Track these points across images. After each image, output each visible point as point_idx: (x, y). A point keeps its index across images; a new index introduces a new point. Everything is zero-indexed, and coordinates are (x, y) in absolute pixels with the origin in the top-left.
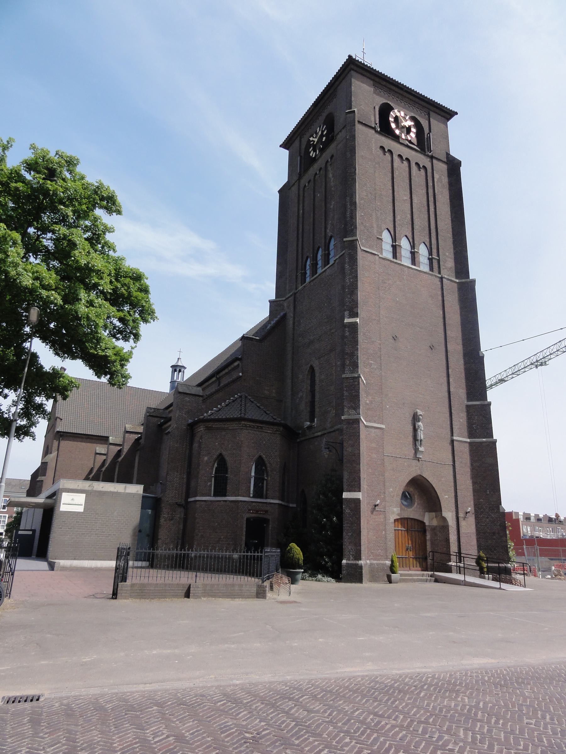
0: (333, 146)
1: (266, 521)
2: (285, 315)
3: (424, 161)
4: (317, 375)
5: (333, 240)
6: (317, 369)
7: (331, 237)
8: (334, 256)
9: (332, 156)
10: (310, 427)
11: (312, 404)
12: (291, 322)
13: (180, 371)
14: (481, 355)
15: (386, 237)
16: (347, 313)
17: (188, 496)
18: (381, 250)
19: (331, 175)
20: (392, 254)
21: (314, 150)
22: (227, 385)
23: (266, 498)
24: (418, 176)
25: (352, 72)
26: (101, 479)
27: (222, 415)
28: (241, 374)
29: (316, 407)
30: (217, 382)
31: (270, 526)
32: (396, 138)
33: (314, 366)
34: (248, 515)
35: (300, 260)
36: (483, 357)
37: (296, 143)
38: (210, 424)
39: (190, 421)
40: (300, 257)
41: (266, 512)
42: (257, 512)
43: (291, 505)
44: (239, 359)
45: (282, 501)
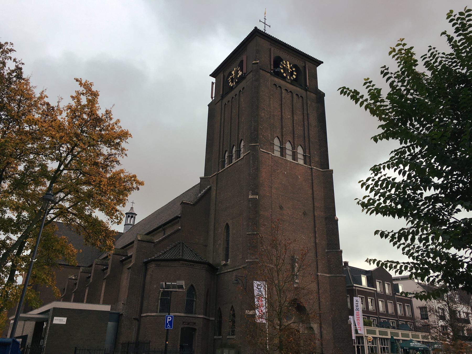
0: (244, 81)
1: (195, 330)
2: (210, 188)
3: (302, 92)
4: (231, 230)
5: (243, 142)
6: (230, 226)
7: (242, 140)
8: (244, 153)
9: (243, 88)
10: (225, 265)
11: (227, 249)
12: (214, 193)
13: (132, 217)
14: (336, 219)
15: (276, 142)
16: (250, 192)
17: (141, 313)
18: (273, 151)
19: (242, 100)
20: (280, 153)
21: (232, 82)
22: (169, 236)
23: (195, 314)
24: (298, 103)
25: (257, 37)
26: (85, 301)
27: (167, 256)
28: (180, 228)
29: (229, 251)
30: (163, 232)
31: (197, 333)
32: (284, 78)
33: (229, 223)
34: (182, 326)
35: (221, 153)
36: (337, 220)
37: (221, 75)
38: (159, 263)
39: (145, 260)
40: (221, 150)
41: (195, 323)
42: (188, 324)
43: (211, 319)
44: (180, 217)
45: (206, 316)
